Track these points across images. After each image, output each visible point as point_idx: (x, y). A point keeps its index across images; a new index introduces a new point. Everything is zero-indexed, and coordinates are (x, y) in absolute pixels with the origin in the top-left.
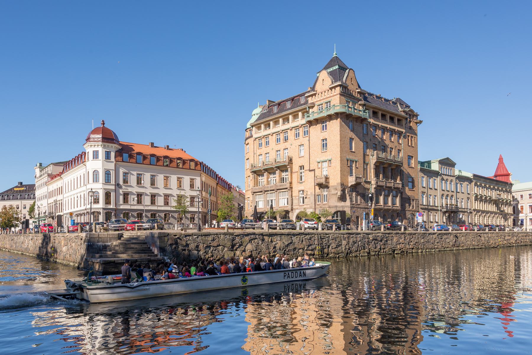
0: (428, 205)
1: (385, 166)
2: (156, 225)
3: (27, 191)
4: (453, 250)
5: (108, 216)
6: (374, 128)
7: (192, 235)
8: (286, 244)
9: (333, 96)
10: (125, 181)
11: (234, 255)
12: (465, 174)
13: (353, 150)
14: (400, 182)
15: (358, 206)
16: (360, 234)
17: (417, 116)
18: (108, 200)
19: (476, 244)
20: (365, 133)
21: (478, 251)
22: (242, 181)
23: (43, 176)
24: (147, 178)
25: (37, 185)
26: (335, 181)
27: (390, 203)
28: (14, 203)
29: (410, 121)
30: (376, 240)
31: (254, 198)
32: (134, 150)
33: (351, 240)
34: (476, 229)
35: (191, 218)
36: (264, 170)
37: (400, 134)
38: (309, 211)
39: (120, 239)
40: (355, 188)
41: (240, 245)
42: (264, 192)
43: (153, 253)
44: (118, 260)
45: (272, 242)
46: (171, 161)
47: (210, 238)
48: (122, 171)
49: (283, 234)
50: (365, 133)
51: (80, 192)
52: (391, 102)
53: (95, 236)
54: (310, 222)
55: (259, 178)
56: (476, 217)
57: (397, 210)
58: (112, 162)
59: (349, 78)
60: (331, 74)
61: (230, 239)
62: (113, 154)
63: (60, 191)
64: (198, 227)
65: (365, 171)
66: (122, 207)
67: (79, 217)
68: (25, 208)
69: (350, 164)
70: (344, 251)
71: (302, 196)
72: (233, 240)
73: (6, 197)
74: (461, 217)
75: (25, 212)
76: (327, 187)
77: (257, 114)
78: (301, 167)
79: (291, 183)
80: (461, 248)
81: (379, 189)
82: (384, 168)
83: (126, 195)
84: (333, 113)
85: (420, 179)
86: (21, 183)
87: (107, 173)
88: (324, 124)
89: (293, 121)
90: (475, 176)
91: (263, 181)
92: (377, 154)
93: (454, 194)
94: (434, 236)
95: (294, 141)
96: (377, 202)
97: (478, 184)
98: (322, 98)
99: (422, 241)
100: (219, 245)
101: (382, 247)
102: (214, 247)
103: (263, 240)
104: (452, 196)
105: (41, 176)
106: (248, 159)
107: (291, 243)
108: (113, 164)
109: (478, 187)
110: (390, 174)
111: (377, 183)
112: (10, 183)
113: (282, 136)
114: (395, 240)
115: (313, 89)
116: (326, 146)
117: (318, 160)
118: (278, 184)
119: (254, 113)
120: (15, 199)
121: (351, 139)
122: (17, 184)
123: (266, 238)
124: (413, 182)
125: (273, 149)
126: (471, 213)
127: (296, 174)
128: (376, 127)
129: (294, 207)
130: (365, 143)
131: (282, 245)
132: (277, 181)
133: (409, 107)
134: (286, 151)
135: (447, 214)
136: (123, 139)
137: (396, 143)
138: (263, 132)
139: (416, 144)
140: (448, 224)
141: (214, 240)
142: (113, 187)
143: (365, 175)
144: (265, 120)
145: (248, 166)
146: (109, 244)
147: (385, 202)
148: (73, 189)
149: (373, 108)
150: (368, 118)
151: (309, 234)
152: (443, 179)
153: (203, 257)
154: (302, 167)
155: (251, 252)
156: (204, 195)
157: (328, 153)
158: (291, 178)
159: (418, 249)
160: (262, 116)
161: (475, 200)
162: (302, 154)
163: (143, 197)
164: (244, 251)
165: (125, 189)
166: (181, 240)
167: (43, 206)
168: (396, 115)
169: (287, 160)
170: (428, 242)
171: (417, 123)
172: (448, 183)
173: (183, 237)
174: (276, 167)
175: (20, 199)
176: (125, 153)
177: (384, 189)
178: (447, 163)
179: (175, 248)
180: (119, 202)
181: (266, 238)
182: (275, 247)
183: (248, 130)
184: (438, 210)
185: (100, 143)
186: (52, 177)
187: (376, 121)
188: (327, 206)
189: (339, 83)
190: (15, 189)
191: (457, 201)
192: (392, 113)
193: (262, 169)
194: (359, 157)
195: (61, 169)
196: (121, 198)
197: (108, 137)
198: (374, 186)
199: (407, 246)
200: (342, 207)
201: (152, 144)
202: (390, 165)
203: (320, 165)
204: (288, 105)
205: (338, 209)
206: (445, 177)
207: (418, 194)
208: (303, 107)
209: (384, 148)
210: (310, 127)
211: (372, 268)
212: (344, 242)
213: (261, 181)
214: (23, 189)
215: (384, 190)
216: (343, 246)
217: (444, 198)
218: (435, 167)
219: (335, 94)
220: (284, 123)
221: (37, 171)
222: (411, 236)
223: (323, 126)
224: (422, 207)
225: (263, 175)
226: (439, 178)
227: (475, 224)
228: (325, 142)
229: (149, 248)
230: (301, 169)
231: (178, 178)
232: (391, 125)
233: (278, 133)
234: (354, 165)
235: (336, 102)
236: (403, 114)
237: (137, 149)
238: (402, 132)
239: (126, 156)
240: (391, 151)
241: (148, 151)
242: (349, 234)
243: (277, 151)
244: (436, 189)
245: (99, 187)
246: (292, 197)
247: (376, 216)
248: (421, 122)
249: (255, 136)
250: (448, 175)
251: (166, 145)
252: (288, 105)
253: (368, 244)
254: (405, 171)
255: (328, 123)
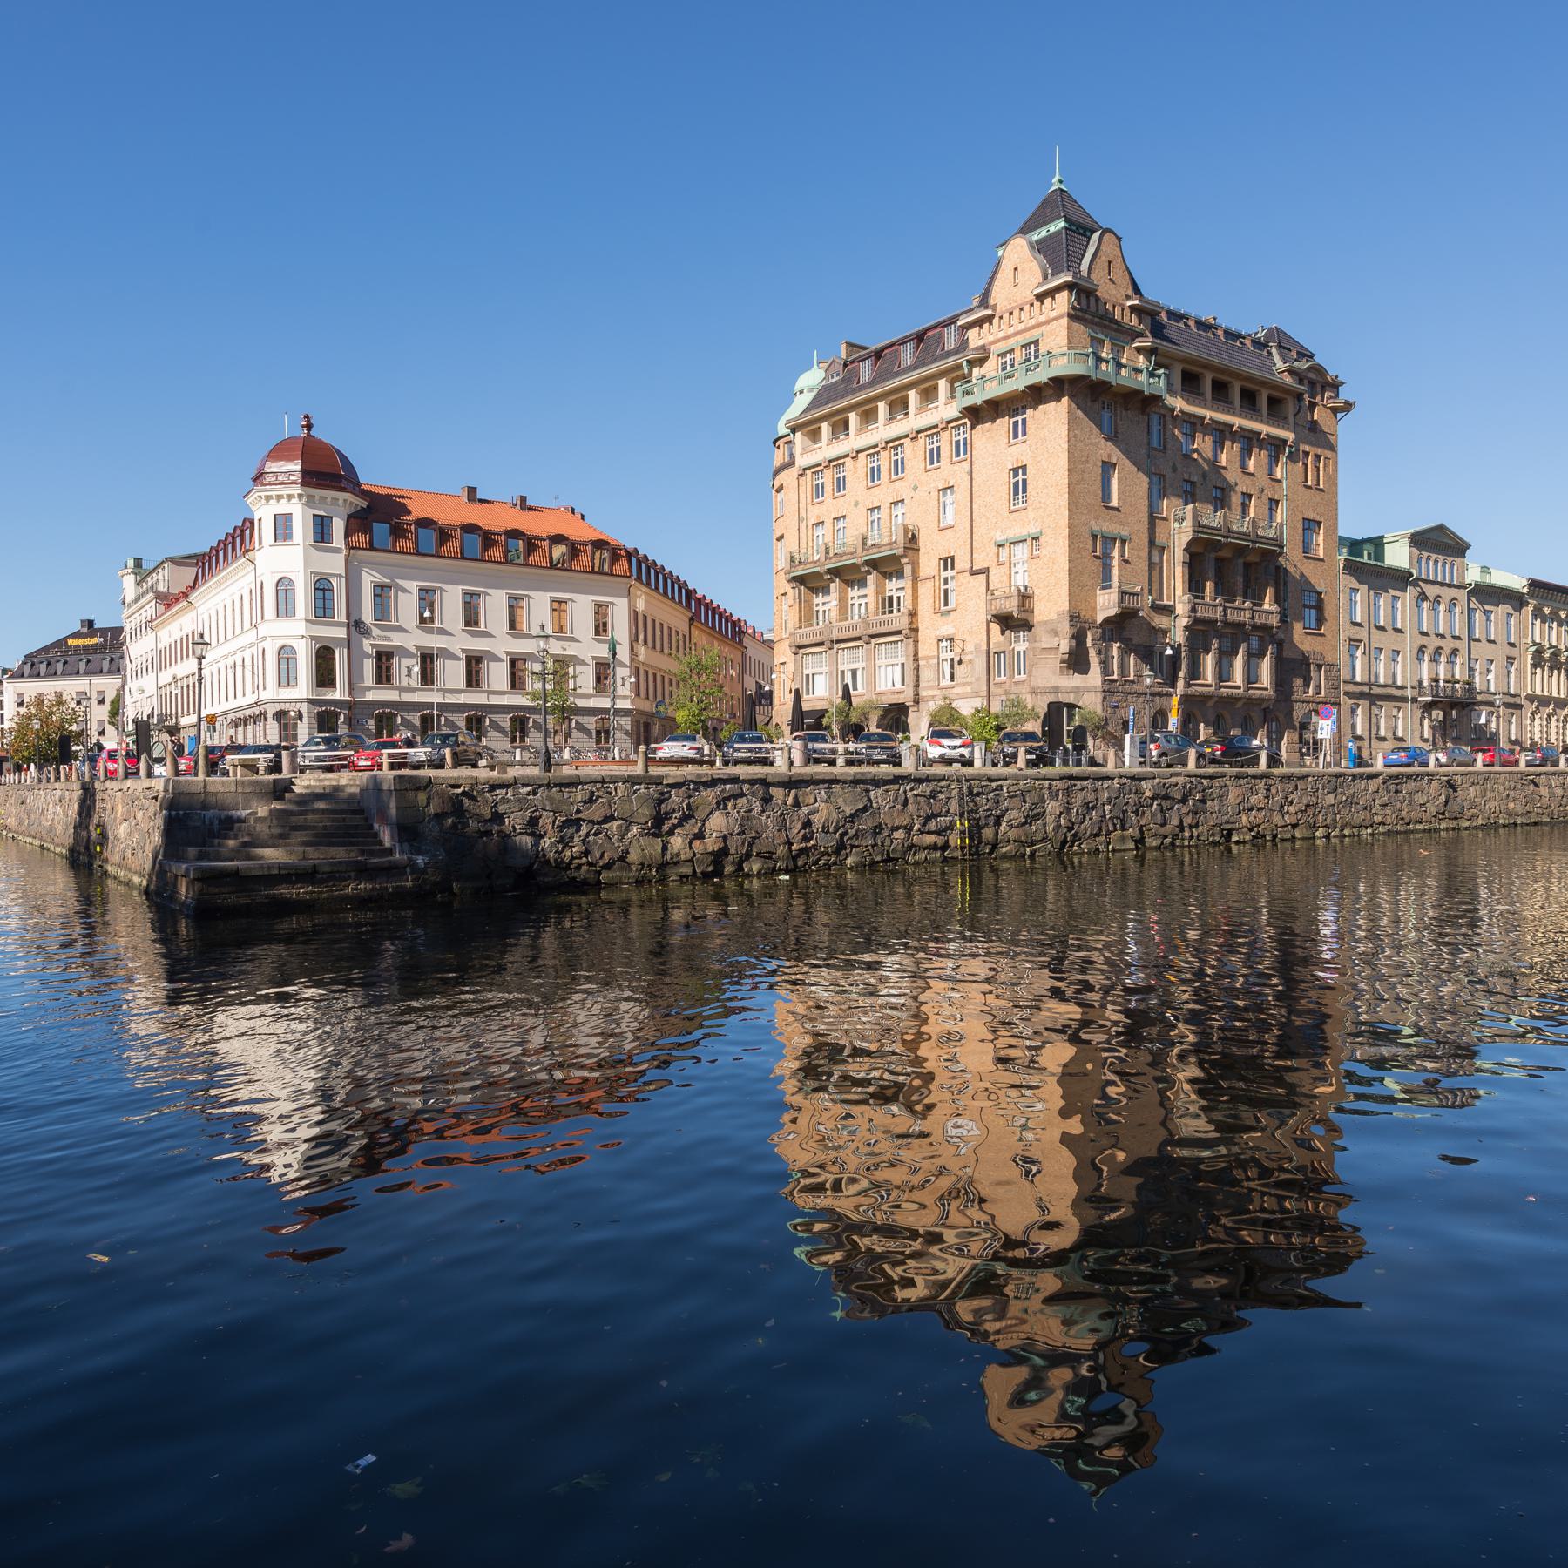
0: (1369, 684)
1: (1225, 553)
2: (447, 751)
3: (100, 649)
4: (1437, 830)
5: (325, 721)
6: (1187, 428)
7: (514, 784)
8: (848, 813)
9: (1048, 322)
10: (382, 611)
11: (665, 848)
12: (1501, 578)
13: (1115, 503)
14: (1274, 608)
15: (1127, 688)
16: (1108, 778)
17: (1335, 386)
18: (324, 677)
19: (1520, 809)
20: (1155, 444)
21: (1528, 833)
22: (771, 612)
23: (143, 601)
24: (452, 600)
25: (127, 630)
26: (1051, 606)
27: (1238, 678)
28: (70, 687)
29: (1313, 406)
30: (1166, 797)
31: (799, 666)
32: (409, 512)
33: (1078, 799)
34: (1523, 759)
35: (598, 733)
36: (829, 571)
37: (1275, 447)
38: (966, 708)
39: (280, 798)
40: (1122, 626)
41: (685, 819)
42: (828, 644)
43: (381, 843)
44: (250, 869)
45: (797, 805)
46: (532, 545)
47: (579, 795)
48: (368, 579)
49: (836, 781)
50: (1155, 444)
51: (242, 649)
52: (1248, 342)
53: (193, 789)
54: (945, 742)
55: (816, 601)
56: (1537, 722)
57: (1261, 700)
58: (337, 551)
59: (1102, 261)
60: (1041, 247)
61: (647, 798)
62: (338, 526)
63: (198, 643)
64: (540, 760)
65: (1155, 573)
66: (370, 696)
67: (240, 730)
68: (101, 702)
69: (1104, 548)
70: (1051, 834)
71: (950, 655)
72: (661, 802)
73: (43, 668)
74: (1483, 721)
75: (101, 713)
76: (1027, 626)
77: (810, 389)
78: (945, 560)
79: (913, 614)
80: (1467, 824)
81: (1201, 632)
82: (1218, 559)
83: (384, 660)
84: (1044, 380)
85: (1343, 599)
86: (91, 623)
87: (322, 588)
88: (1019, 418)
89: (920, 410)
90: (1534, 584)
91: (826, 607)
92: (1195, 516)
93: (1462, 645)
94: (1373, 785)
95: (924, 477)
96: (1195, 672)
97: (1547, 611)
98: (1011, 330)
99: (1330, 799)
100: (609, 818)
101: (1188, 820)
102: (592, 822)
103: (767, 800)
104: (1455, 652)
105: (138, 599)
106: (781, 538)
107: (865, 809)
108: (341, 558)
109: (1543, 621)
110: (1240, 579)
111: (1194, 610)
112: (59, 625)
113: (885, 461)
114: (1233, 796)
115: (984, 302)
116: (1024, 491)
117: (1000, 538)
118: (873, 618)
119: (798, 386)
120: (70, 674)
121: (1108, 467)
122: (78, 627)
123: (777, 793)
124: (1319, 607)
125: (856, 504)
126: (1520, 707)
127: (930, 584)
128: (1193, 424)
129: (923, 693)
130: (1155, 479)
131: (834, 817)
132: (872, 607)
133: (1311, 356)
134: (899, 510)
135: (1438, 714)
136: (374, 477)
137: (1262, 479)
138: (827, 449)
139: (1333, 480)
140: (1440, 744)
141: (591, 800)
142: (341, 633)
143: (1155, 587)
144: (830, 413)
145: (781, 562)
146: (244, 813)
147: (1223, 674)
148: (230, 635)
149: (1184, 360)
150: (1164, 394)
151: (928, 779)
152: (1423, 597)
153: (551, 856)
154: (948, 562)
155: (725, 838)
156: (641, 658)
157: (1030, 513)
158: (915, 598)
159: (1314, 826)
160: (825, 395)
161: (1535, 666)
162: (949, 519)
163: (483, 665)
164: (700, 835)
165: (381, 638)
166: (475, 799)
167: (142, 698)
168: (1264, 384)
169: (901, 540)
170: (1350, 803)
171: (1335, 410)
172: (1442, 608)
173: (481, 792)
174: (867, 563)
175: (87, 673)
176: (379, 520)
177: (1217, 631)
178: (1439, 542)
179: (454, 825)
180: (362, 679)
181: (777, 793)
182: (807, 824)
183: (780, 443)
184: (1404, 699)
185: (296, 490)
186: (167, 600)
187: (1188, 403)
188: (1025, 689)
189: (1066, 278)
190: (70, 642)
191: (1471, 670)
192: (1250, 379)
193: (822, 570)
194: (1135, 526)
195: (189, 573)
196: (369, 666)
197: (324, 470)
198: (1185, 621)
199: (1277, 819)
200: (1077, 690)
201: (472, 492)
202: (1241, 550)
203: (1004, 552)
204: (907, 355)
205: (1063, 698)
206: (1431, 591)
207: (1335, 648)
208: (951, 361)
209: (1221, 496)
210: (973, 428)
211: (1151, 886)
212: (1052, 807)
213: (821, 608)
214: (94, 641)
215: (1246, 639)
216: (1050, 819)
217: (1427, 658)
218: (1398, 555)
219: (1053, 314)
220: (891, 417)
221: (129, 582)
222: (1291, 787)
223: (1016, 423)
224: (1351, 688)
225: (826, 591)
226: (1410, 594)
227: (1533, 744)
228: (1021, 477)
229: (371, 827)
230: (945, 569)
231: (599, 605)
232: (1217, 411)
233: (872, 451)
234: (1116, 553)
235: (1058, 345)
236: (1288, 380)
237: (418, 509)
238: (1285, 441)
239: (381, 529)
240: (1245, 506)
241: (454, 514)
242: (1071, 778)
243: (872, 510)
244: (1399, 631)
245: (297, 631)
246: (916, 659)
247: (1188, 720)
248: (1348, 407)
249: (802, 461)
250: (1442, 584)
251: (517, 494)
252: (907, 355)
253: (1136, 813)
254: (1291, 569)
255: (1029, 412)
